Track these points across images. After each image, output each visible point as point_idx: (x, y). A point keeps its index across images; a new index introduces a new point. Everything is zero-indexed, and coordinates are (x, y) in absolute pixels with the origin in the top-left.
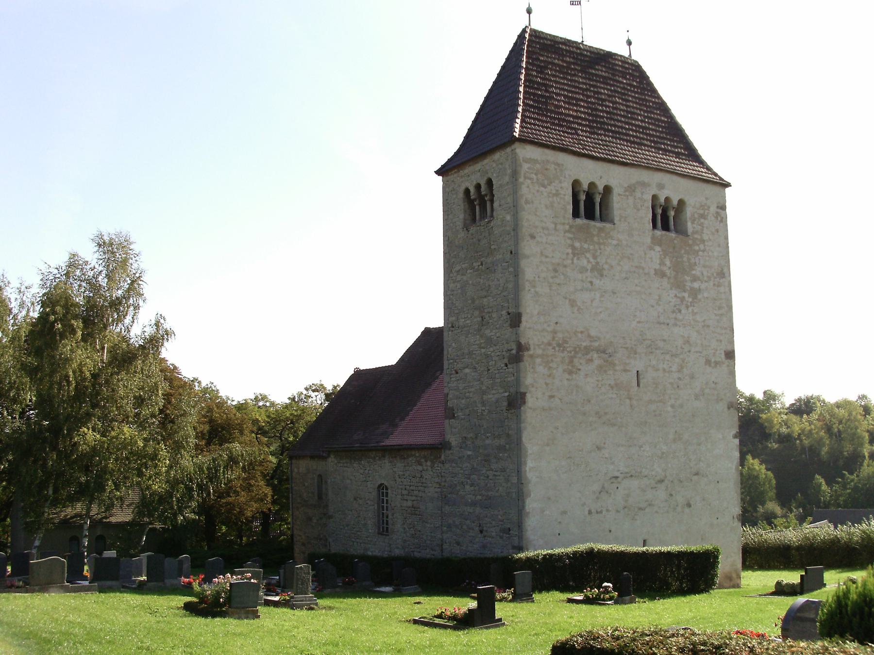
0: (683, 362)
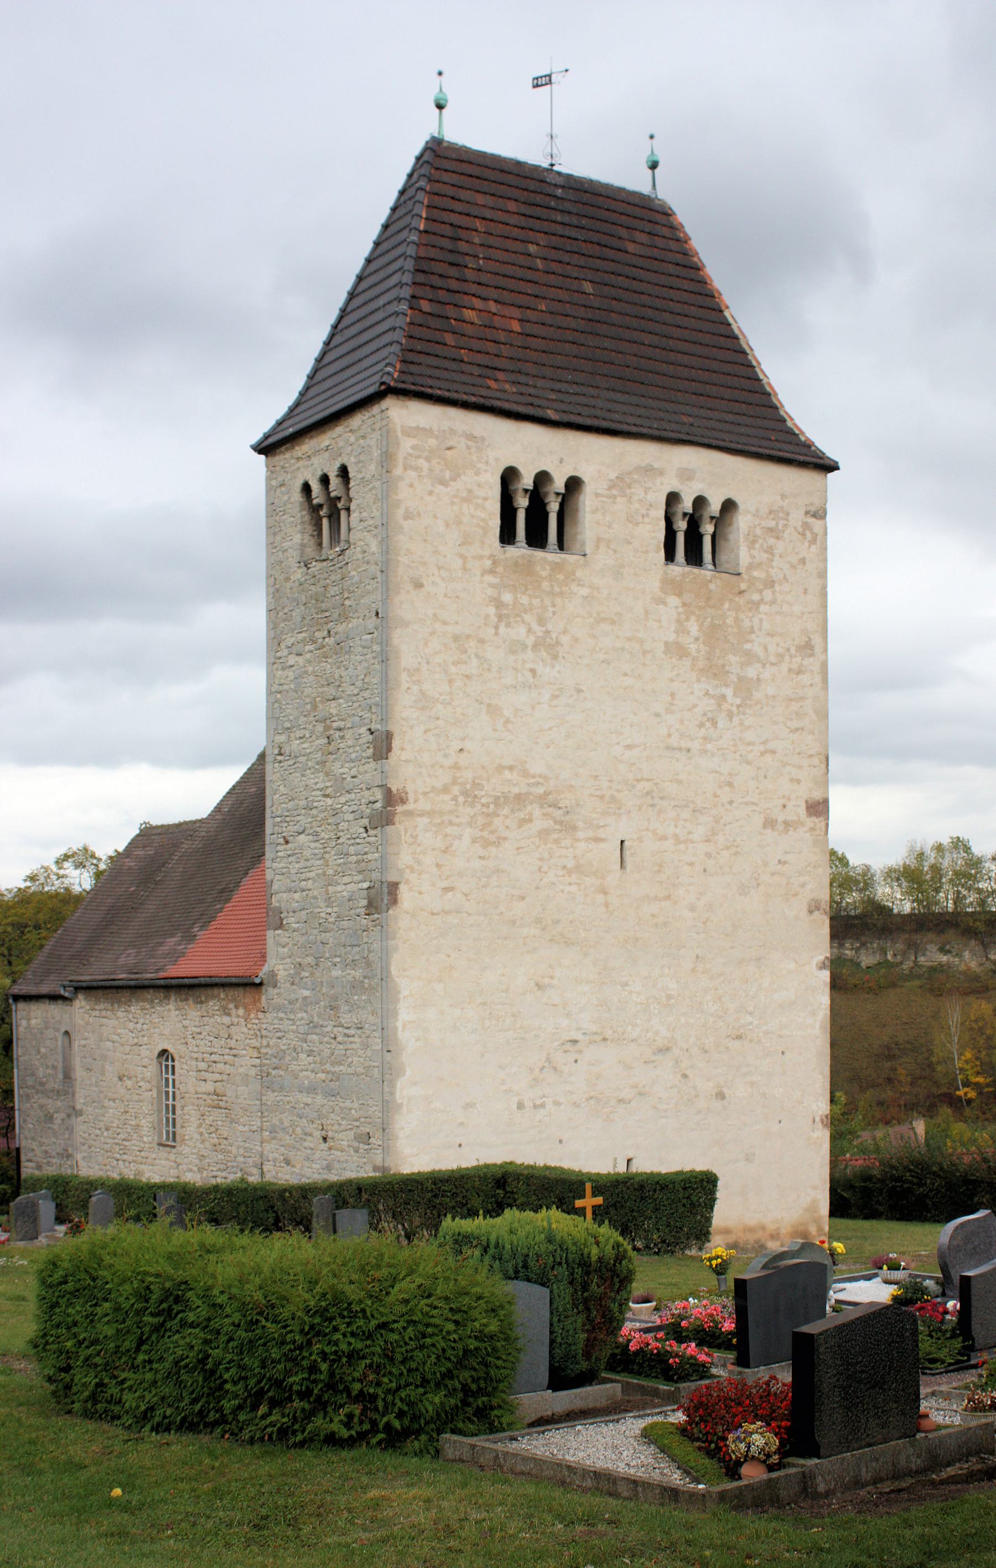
0: (717, 822)
